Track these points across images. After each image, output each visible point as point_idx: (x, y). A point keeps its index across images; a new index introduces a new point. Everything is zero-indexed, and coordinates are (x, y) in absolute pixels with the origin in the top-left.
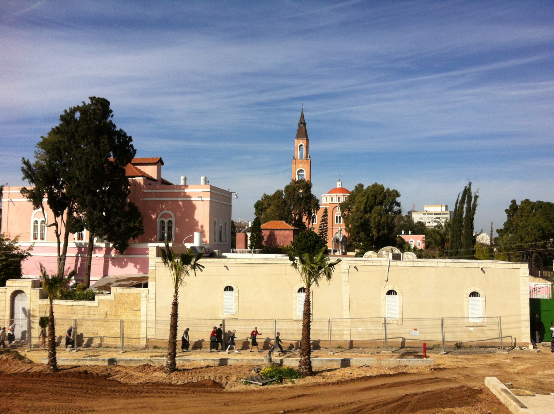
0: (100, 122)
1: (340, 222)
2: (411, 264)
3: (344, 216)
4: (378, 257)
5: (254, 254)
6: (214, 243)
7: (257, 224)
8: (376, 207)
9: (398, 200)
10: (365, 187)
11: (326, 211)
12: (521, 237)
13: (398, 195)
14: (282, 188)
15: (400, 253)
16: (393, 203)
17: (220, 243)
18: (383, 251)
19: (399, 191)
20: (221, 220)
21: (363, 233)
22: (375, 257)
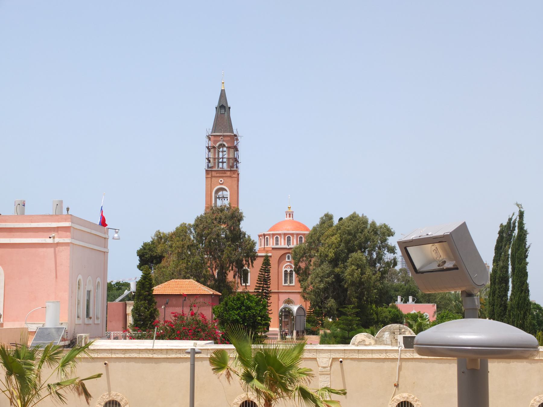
1: (291, 282)
3: (298, 270)
4: (377, 342)
5: (156, 341)
6: (77, 321)
7: (146, 284)
8: (354, 255)
11: (267, 261)
12: (306, 275)
15: (414, 335)
17: (87, 321)
18: (384, 332)
20: (90, 278)
21: (333, 300)
22: (370, 344)
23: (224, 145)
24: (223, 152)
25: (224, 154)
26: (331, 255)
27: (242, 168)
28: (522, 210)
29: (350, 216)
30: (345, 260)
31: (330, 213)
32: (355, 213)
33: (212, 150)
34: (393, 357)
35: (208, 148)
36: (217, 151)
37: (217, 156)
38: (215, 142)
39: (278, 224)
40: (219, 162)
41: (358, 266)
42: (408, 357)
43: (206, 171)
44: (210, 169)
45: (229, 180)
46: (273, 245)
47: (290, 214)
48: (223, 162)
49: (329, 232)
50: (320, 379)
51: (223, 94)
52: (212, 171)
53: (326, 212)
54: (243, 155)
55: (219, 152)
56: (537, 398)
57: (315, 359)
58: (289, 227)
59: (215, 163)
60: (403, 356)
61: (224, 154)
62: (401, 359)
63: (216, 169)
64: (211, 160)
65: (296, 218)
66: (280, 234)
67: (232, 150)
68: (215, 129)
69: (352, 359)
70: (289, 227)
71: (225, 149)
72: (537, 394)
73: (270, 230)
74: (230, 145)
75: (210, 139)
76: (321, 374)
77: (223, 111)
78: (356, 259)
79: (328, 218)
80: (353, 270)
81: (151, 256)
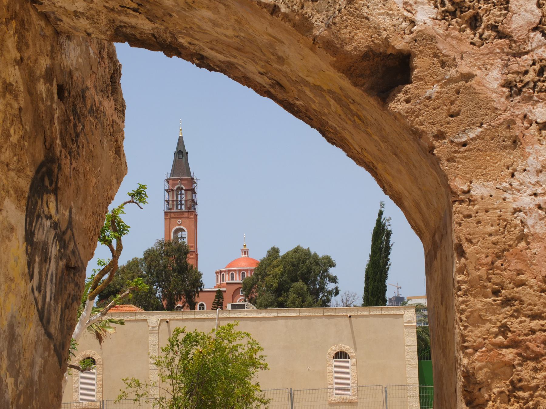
0: (227, 386)
2: (252, 315)
8: (296, 285)
9: (332, 271)
10: (282, 253)
13: (332, 264)
14: (141, 256)
16: (325, 277)
19: (333, 258)
23: (182, 188)
24: (181, 194)
25: (183, 197)
26: (275, 285)
27: (200, 209)
28: (382, 209)
29: (294, 249)
30: (287, 290)
31: (276, 247)
32: (299, 246)
33: (171, 193)
34: (212, 317)
35: (167, 191)
36: (175, 194)
37: (175, 199)
38: (174, 185)
39: (236, 260)
40: (177, 205)
41: (300, 295)
42: (225, 316)
43: (165, 212)
44: (168, 211)
45: (187, 221)
46: (229, 280)
47: (245, 252)
48: (181, 204)
49: (274, 263)
50: (150, 337)
51: (181, 141)
52: (170, 212)
53: (272, 246)
54: (200, 197)
55: (177, 195)
56: (334, 348)
57: (146, 320)
58: (244, 264)
59: (173, 205)
60: (221, 316)
61: (183, 197)
62: (219, 318)
63: (175, 210)
64: (170, 202)
65: (251, 255)
66: (235, 271)
67: (189, 193)
68: (173, 173)
69: (177, 320)
70: (244, 264)
71: (183, 192)
72: (334, 345)
73: (226, 267)
74: (187, 188)
75: (168, 182)
76: (150, 333)
77: (181, 156)
78: (297, 288)
79: (274, 251)
80: (294, 298)
81: (109, 292)
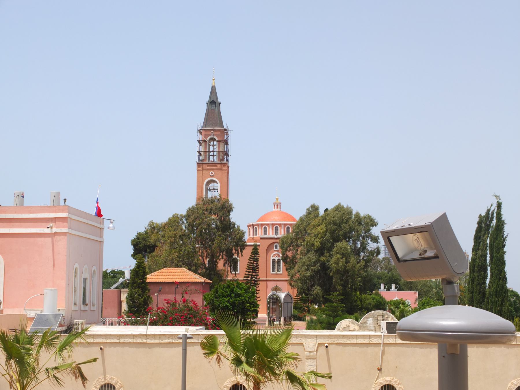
1: (279, 270)
3: (285, 259)
4: (361, 328)
5: (149, 327)
6: (74, 308)
7: (139, 273)
8: (339, 244)
11: (255, 251)
15: (396, 321)
17: (83, 307)
18: (368, 318)
20: (86, 266)
21: (319, 288)
22: (354, 330)
23: (215, 139)
24: (213, 145)
25: (215, 148)
26: (317, 244)
27: (232, 161)
28: (500, 201)
29: (335, 207)
30: (330, 249)
31: (316, 204)
32: (340, 204)
33: (203, 144)
34: (377, 342)
35: (199, 142)
36: (207, 145)
37: (207, 150)
38: (206, 136)
39: (267, 214)
40: (209, 156)
41: (343, 255)
42: (391, 342)
43: (198, 164)
44: (201, 162)
45: (219, 172)
46: (262, 234)
47: (277, 205)
48: (213, 156)
49: (315, 222)
50: (307, 364)
51: (213, 90)
52: (203, 164)
53: (312, 204)
54: (232, 148)
55: (209, 145)
56: (515, 382)
57: (302, 344)
58: (277, 218)
59: (205, 157)
60: (386, 341)
61: (215, 148)
62: (384, 344)
63: (207, 162)
64: (202, 153)
65: (284, 209)
66: (268, 225)
67: (222, 144)
68: (206, 124)
69: (337, 344)
70: (277, 218)
71: (215, 143)
72: (515, 378)
73: (259, 221)
74: (220, 139)
75: (201, 133)
76: (307, 359)
77: (213, 106)
78: (341, 248)
79: (315, 209)
80: (338, 258)
81: (145, 245)
